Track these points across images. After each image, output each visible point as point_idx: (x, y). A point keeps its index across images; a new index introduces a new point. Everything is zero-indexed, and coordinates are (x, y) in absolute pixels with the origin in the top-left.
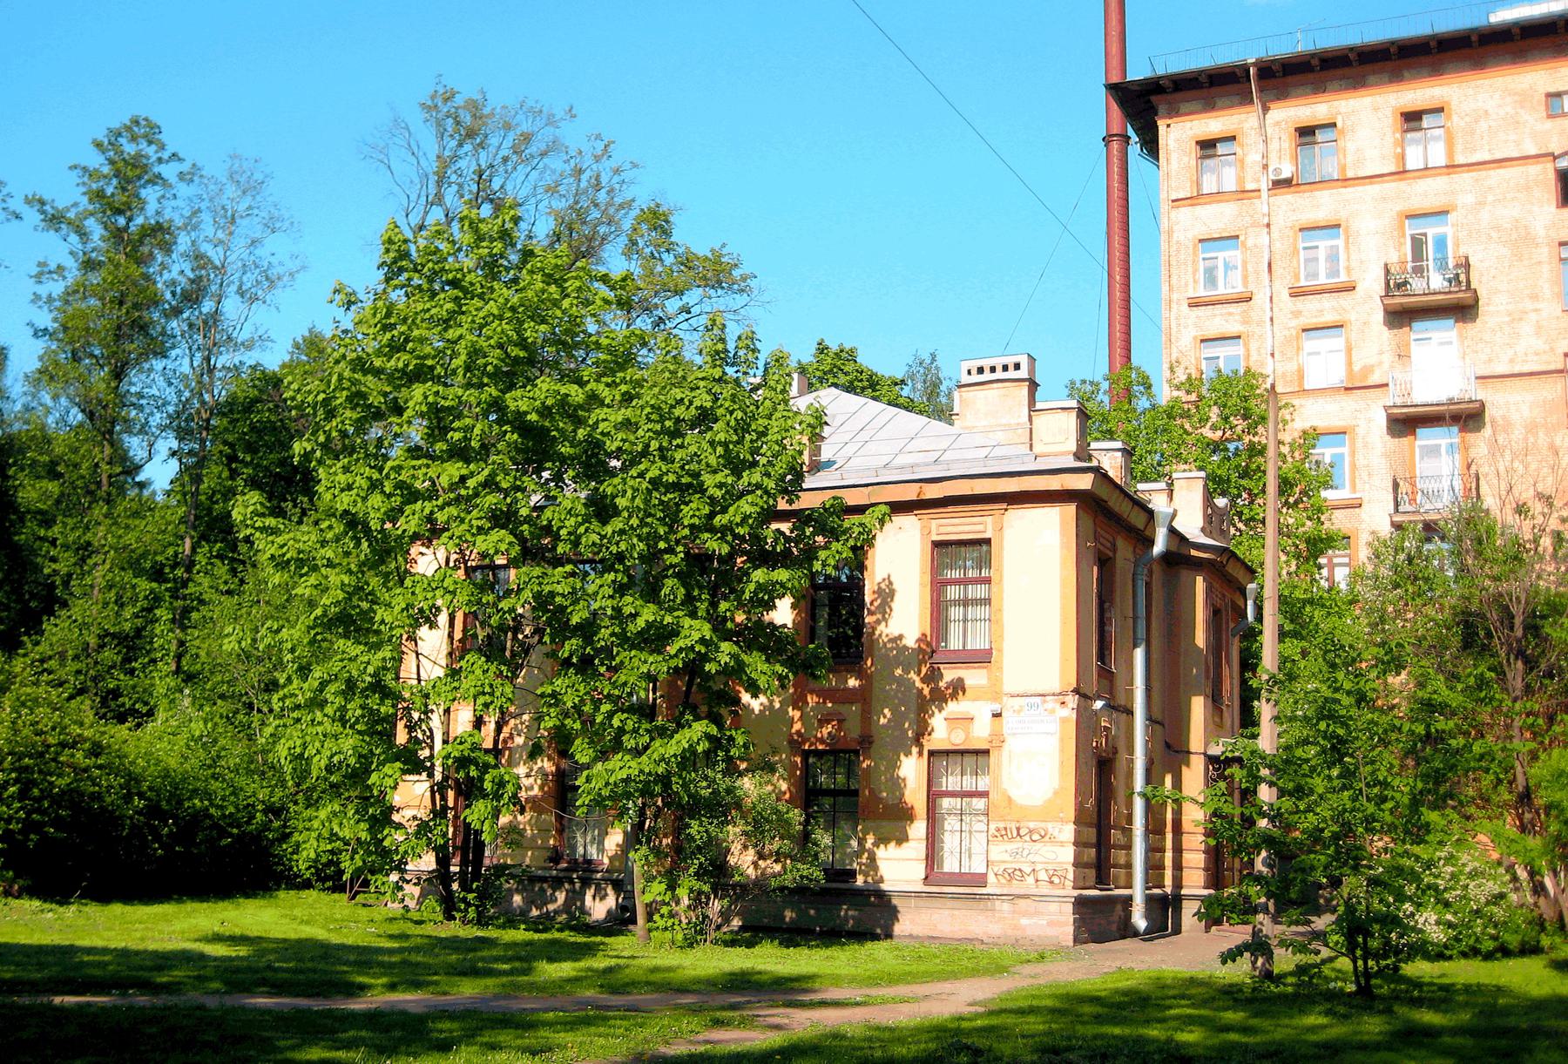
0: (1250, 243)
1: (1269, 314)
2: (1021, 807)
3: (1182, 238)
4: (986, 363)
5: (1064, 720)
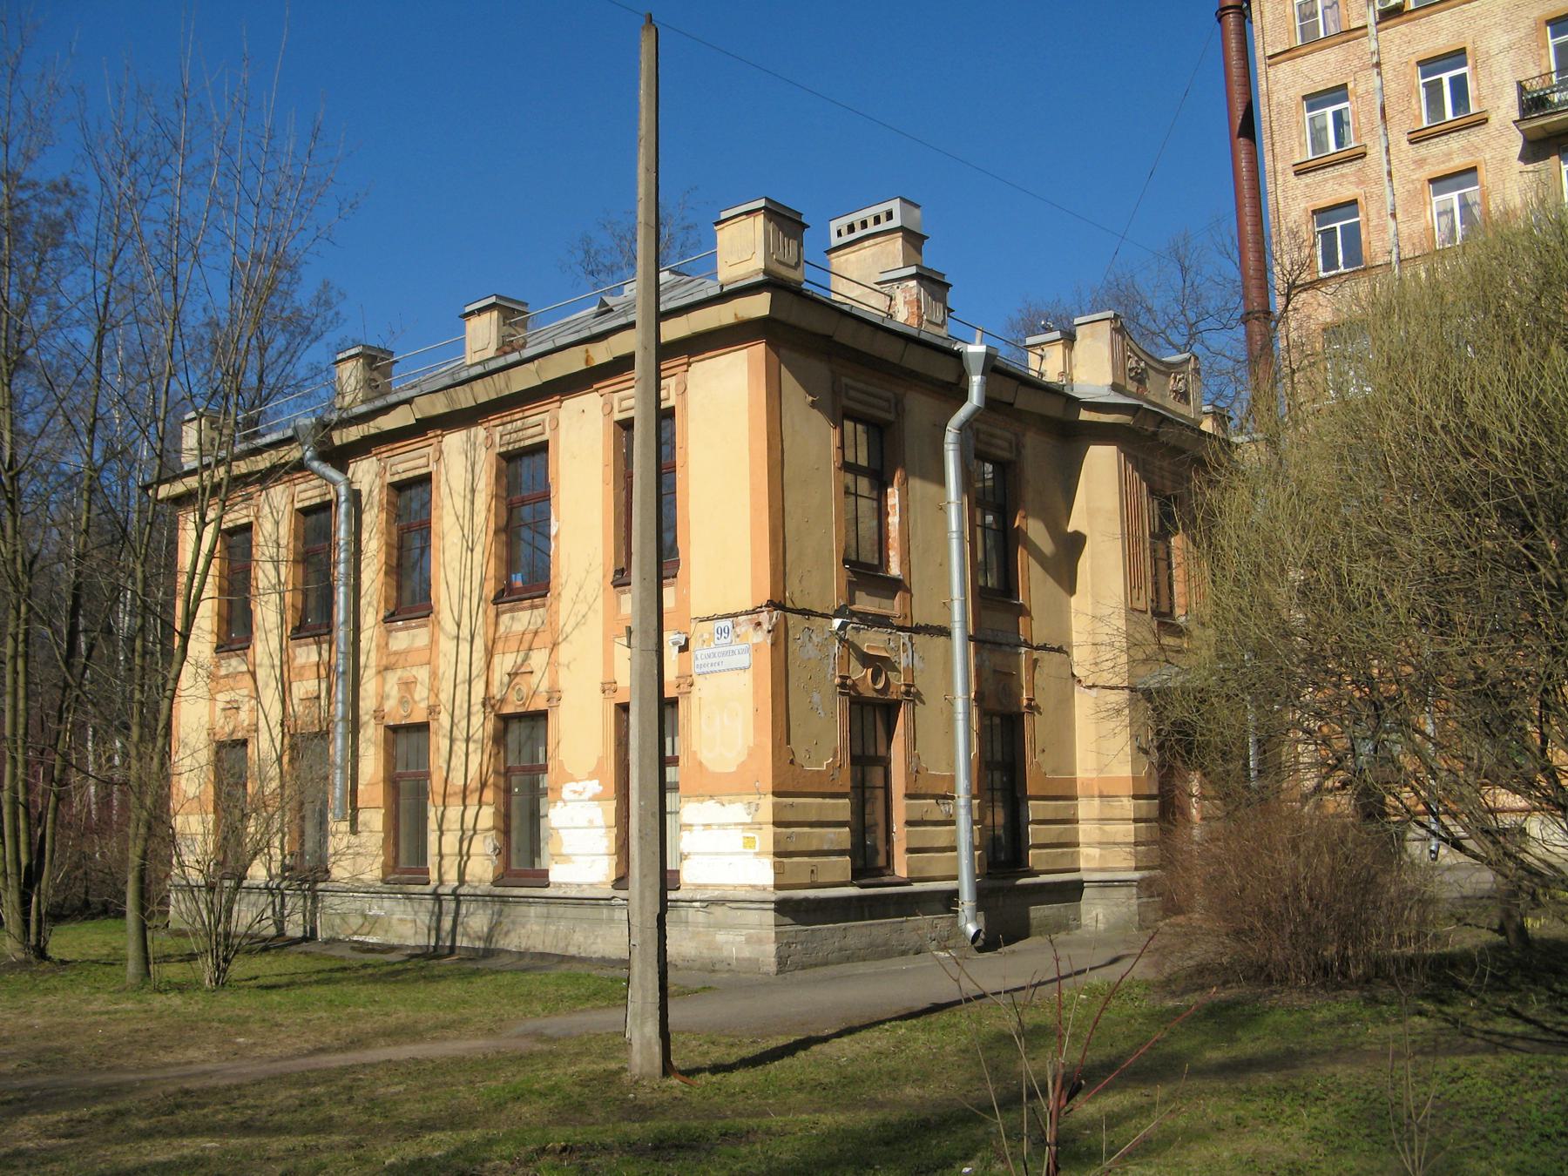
0: (1361, 90)
1: (1385, 167)
3: (1283, 98)
4: (856, 218)
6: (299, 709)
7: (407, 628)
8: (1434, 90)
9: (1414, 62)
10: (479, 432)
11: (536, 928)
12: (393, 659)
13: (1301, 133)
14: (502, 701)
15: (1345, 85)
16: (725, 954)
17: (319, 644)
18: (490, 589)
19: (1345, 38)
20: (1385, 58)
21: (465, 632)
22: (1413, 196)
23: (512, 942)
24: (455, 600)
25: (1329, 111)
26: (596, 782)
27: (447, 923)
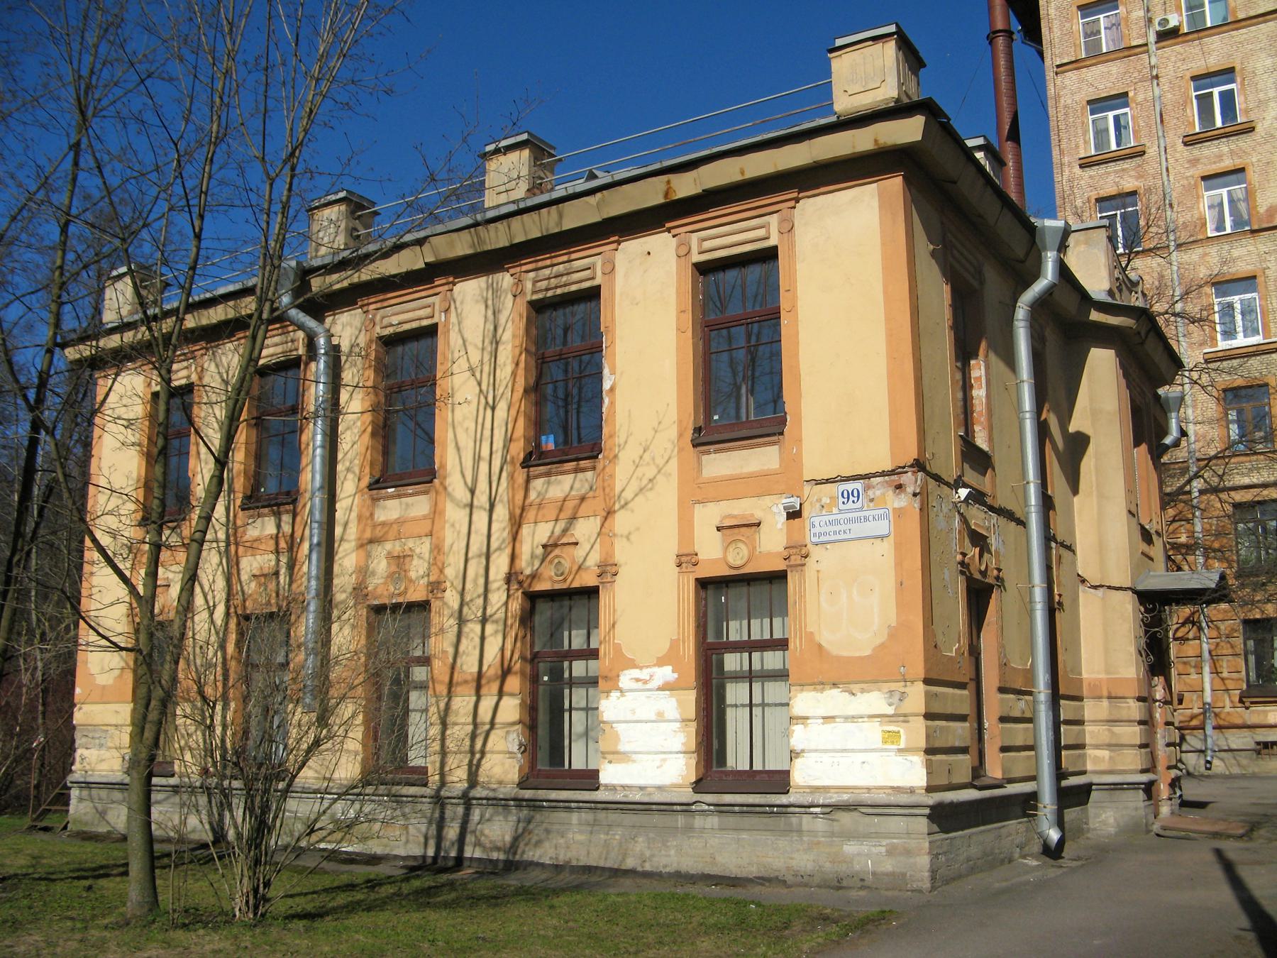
0: (1140, 98)
2: (839, 659)
3: (1069, 102)
5: (899, 513)
6: (251, 588)
7: (399, 496)
8: (1205, 103)
9: (1188, 77)
10: (505, 280)
11: (579, 837)
12: (379, 532)
13: (1085, 132)
14: (534, 576)
15: (1126, 94)
16: (857, 867)
17: (278, 515)
18: (518, 450)
19: (1126, 53)
20: (1162, 72)
21: (482, 499)
22: (1191, 190)
23: (544, 853)
24: (468, 463)
25: (1111, 115)
26: (669, 668)
27: (452, 833)
